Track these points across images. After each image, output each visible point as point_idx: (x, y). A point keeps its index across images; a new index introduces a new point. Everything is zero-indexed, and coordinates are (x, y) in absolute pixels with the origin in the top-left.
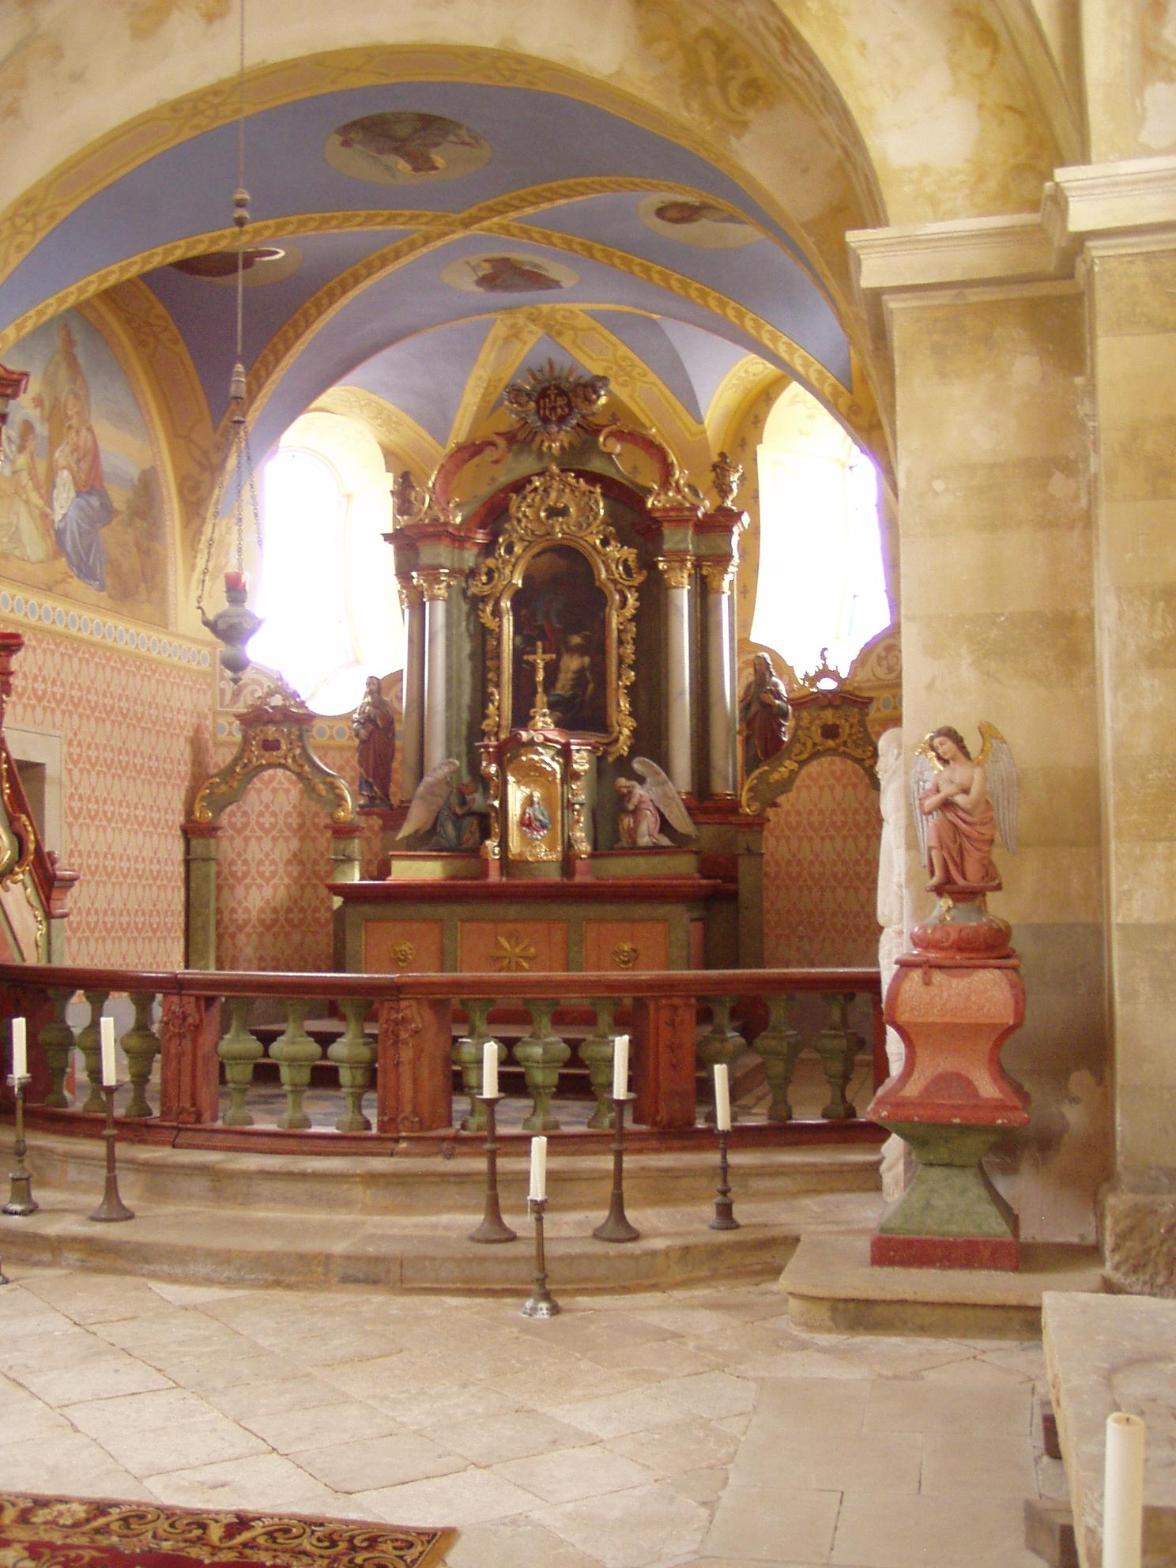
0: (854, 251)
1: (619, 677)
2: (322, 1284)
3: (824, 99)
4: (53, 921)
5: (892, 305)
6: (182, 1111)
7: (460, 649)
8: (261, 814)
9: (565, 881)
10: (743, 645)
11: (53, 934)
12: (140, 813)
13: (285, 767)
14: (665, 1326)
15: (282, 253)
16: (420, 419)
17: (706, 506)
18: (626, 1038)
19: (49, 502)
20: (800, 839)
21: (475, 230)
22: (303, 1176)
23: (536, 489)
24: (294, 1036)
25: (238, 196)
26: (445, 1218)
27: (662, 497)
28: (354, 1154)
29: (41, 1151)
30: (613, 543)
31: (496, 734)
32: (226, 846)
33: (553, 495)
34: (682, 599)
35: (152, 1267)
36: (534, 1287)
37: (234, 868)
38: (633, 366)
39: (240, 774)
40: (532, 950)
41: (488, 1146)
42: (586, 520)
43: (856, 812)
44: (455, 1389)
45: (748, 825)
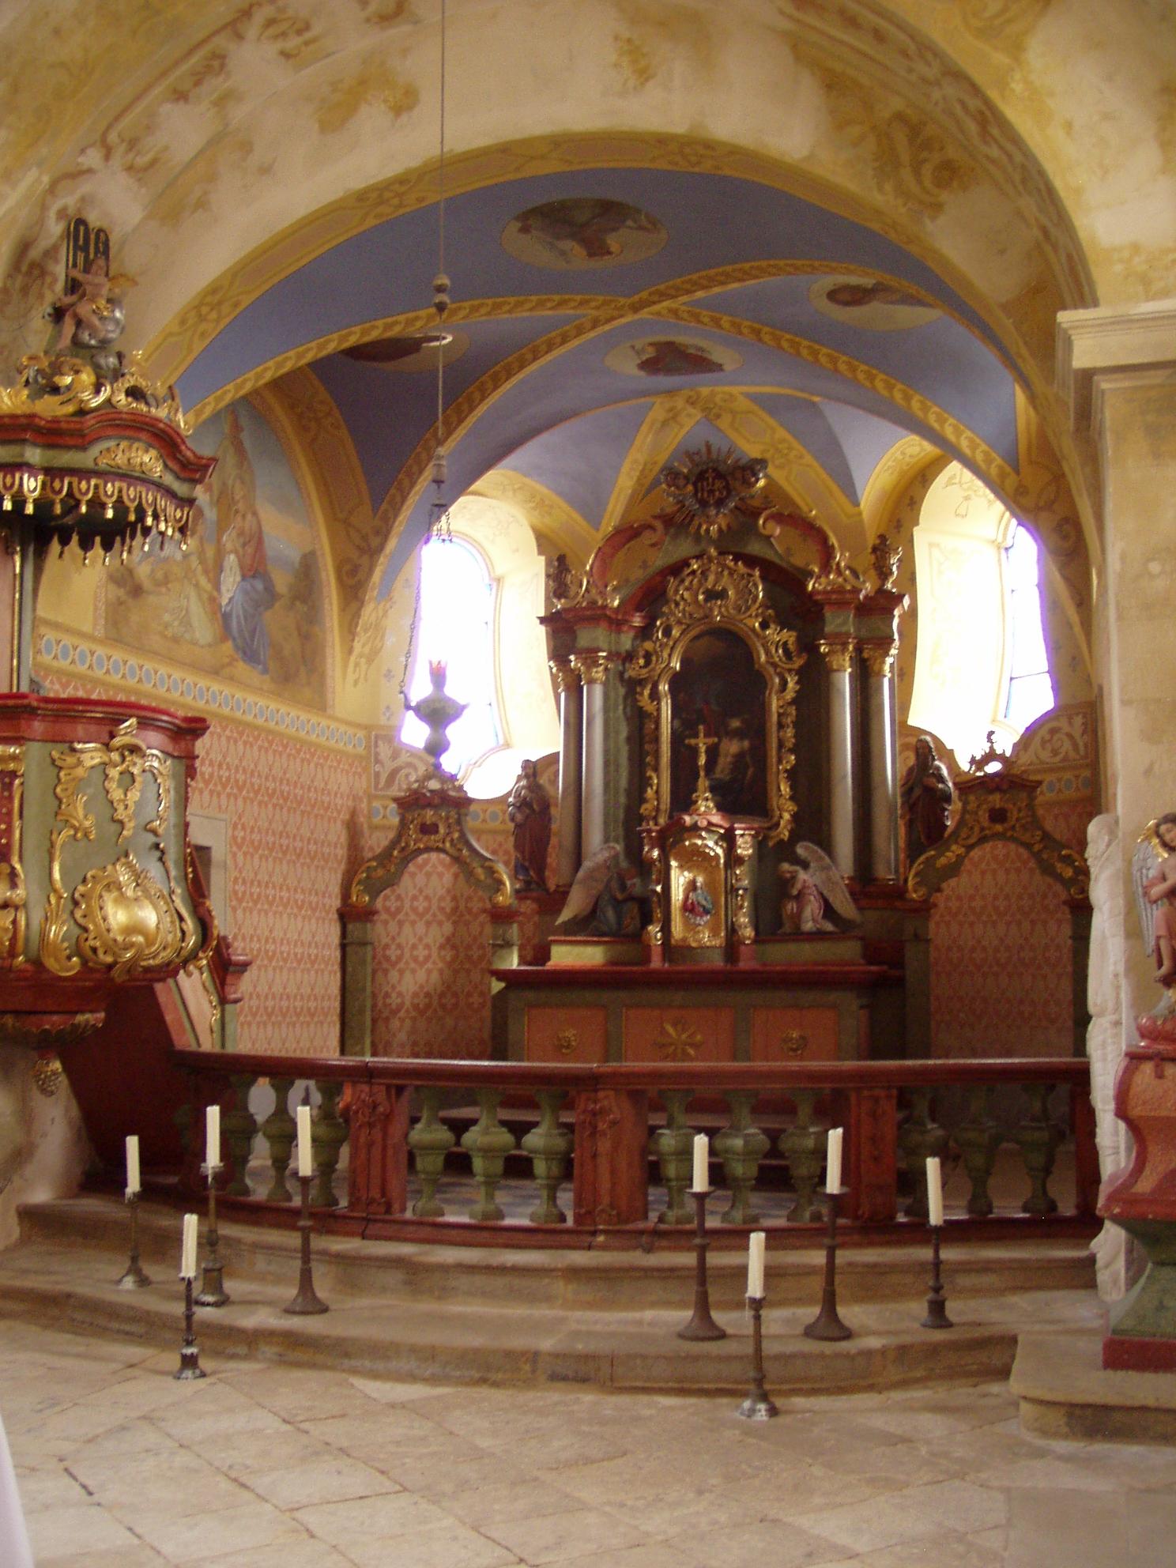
0: (1065, 331)
1: (780, 761)
2: (529, 1383)
3: (1024, 181)
4: (228, 1007)
5: (1104, 386)
6: (371, 1202)
7: (617, 733)
8: (415, 898)
9: (729, 967)
10: (902, 727)
11: (227, 1019)
12: (300, 896)
13: (443, 851)
14: (892, 1429)
15: (449, 339)
16: (571, 501)
17: (868, 588)
18: (840, 1131)
19: (217, 586)
20: (961, 924)
21: (644, 314)
22: (516, 1270)
23: (694, 572)
24: (487, 1128)
25: (439, 282)
26: (649, 1314)
27: (823, 580)
28: (551, 1247)
29: (230, 1242)
30: (772, 626)
31: (655, 818)
32: (380, 931)
33: (711, 578)
34: (844, 681)
35: (353, 1362)
36: (752, 1387)
37: (388, 952)
38: (790, 448)
39: (397, 858)
40: (699, 1037)
41: (698, 1241)
42: (744, 603)
43: (1020, 897)
44: (691, 1495)
45: (916, 911)
